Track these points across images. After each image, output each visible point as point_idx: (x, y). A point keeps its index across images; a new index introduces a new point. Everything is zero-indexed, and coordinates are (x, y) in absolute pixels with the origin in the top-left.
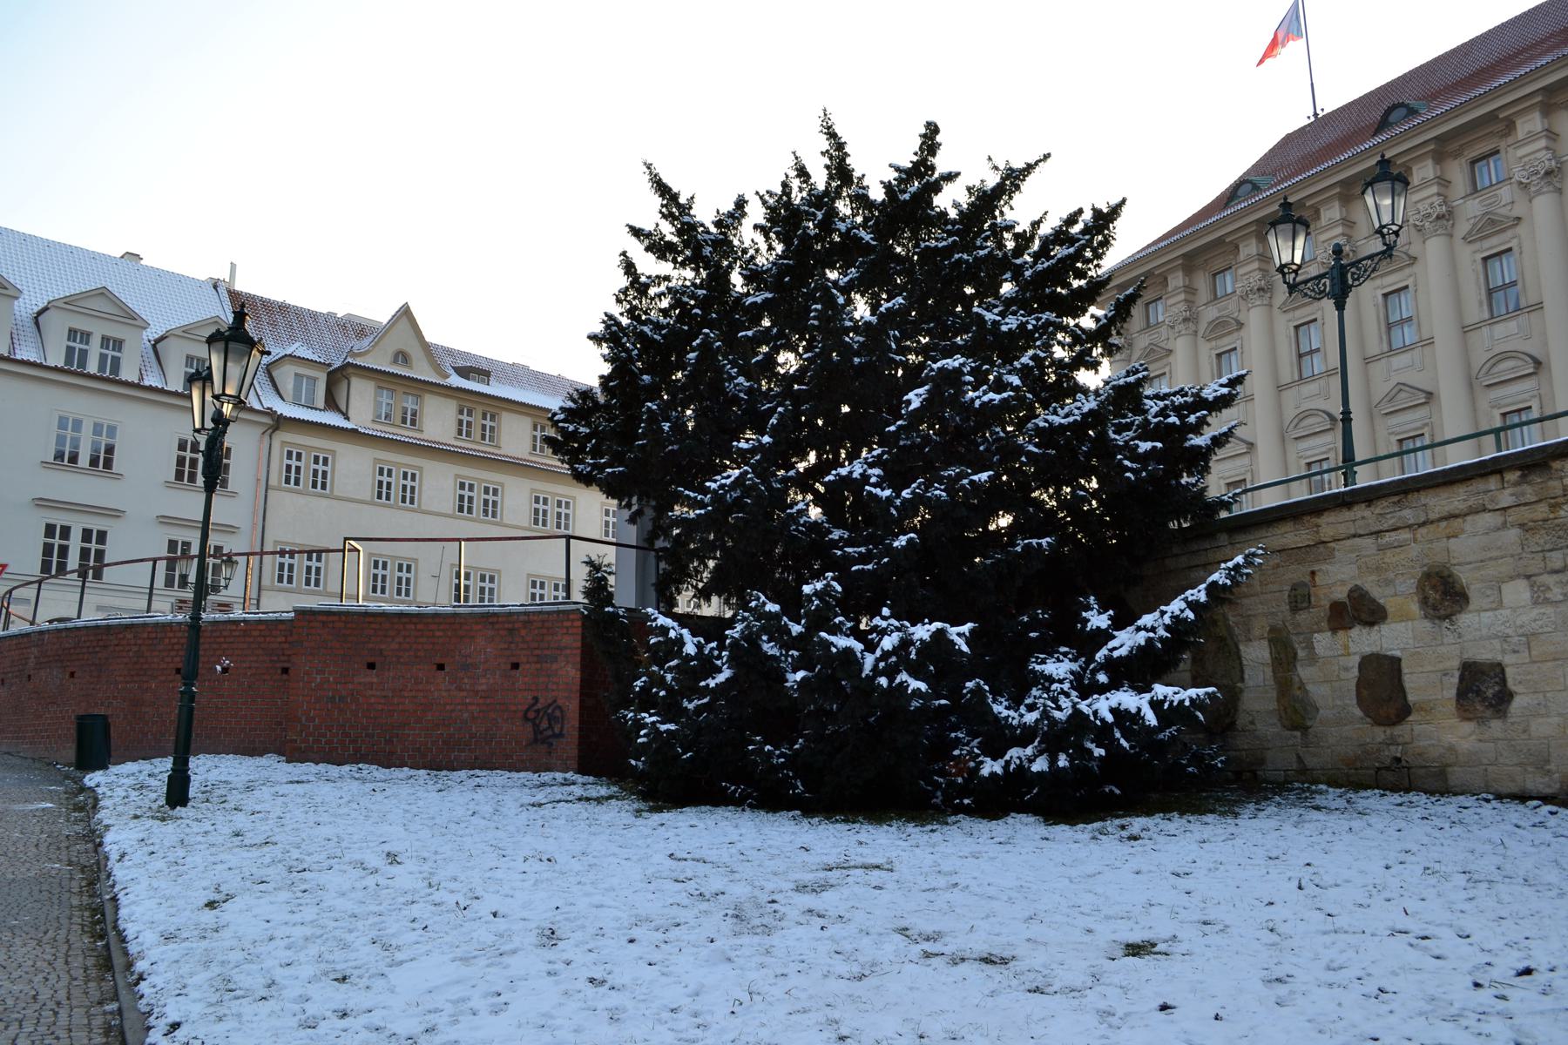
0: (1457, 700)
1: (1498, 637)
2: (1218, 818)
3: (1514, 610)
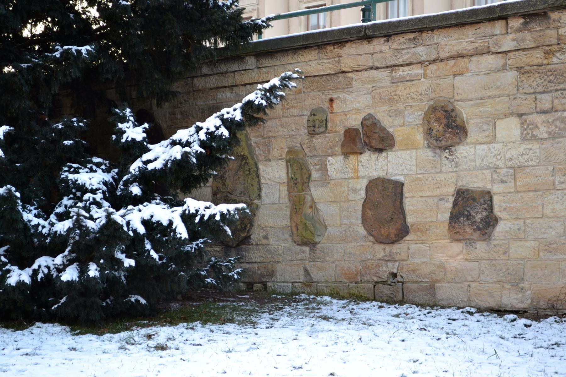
0: (450, 223)
1: (490, 168)
2: (238, 327)
3: (505, 144)
